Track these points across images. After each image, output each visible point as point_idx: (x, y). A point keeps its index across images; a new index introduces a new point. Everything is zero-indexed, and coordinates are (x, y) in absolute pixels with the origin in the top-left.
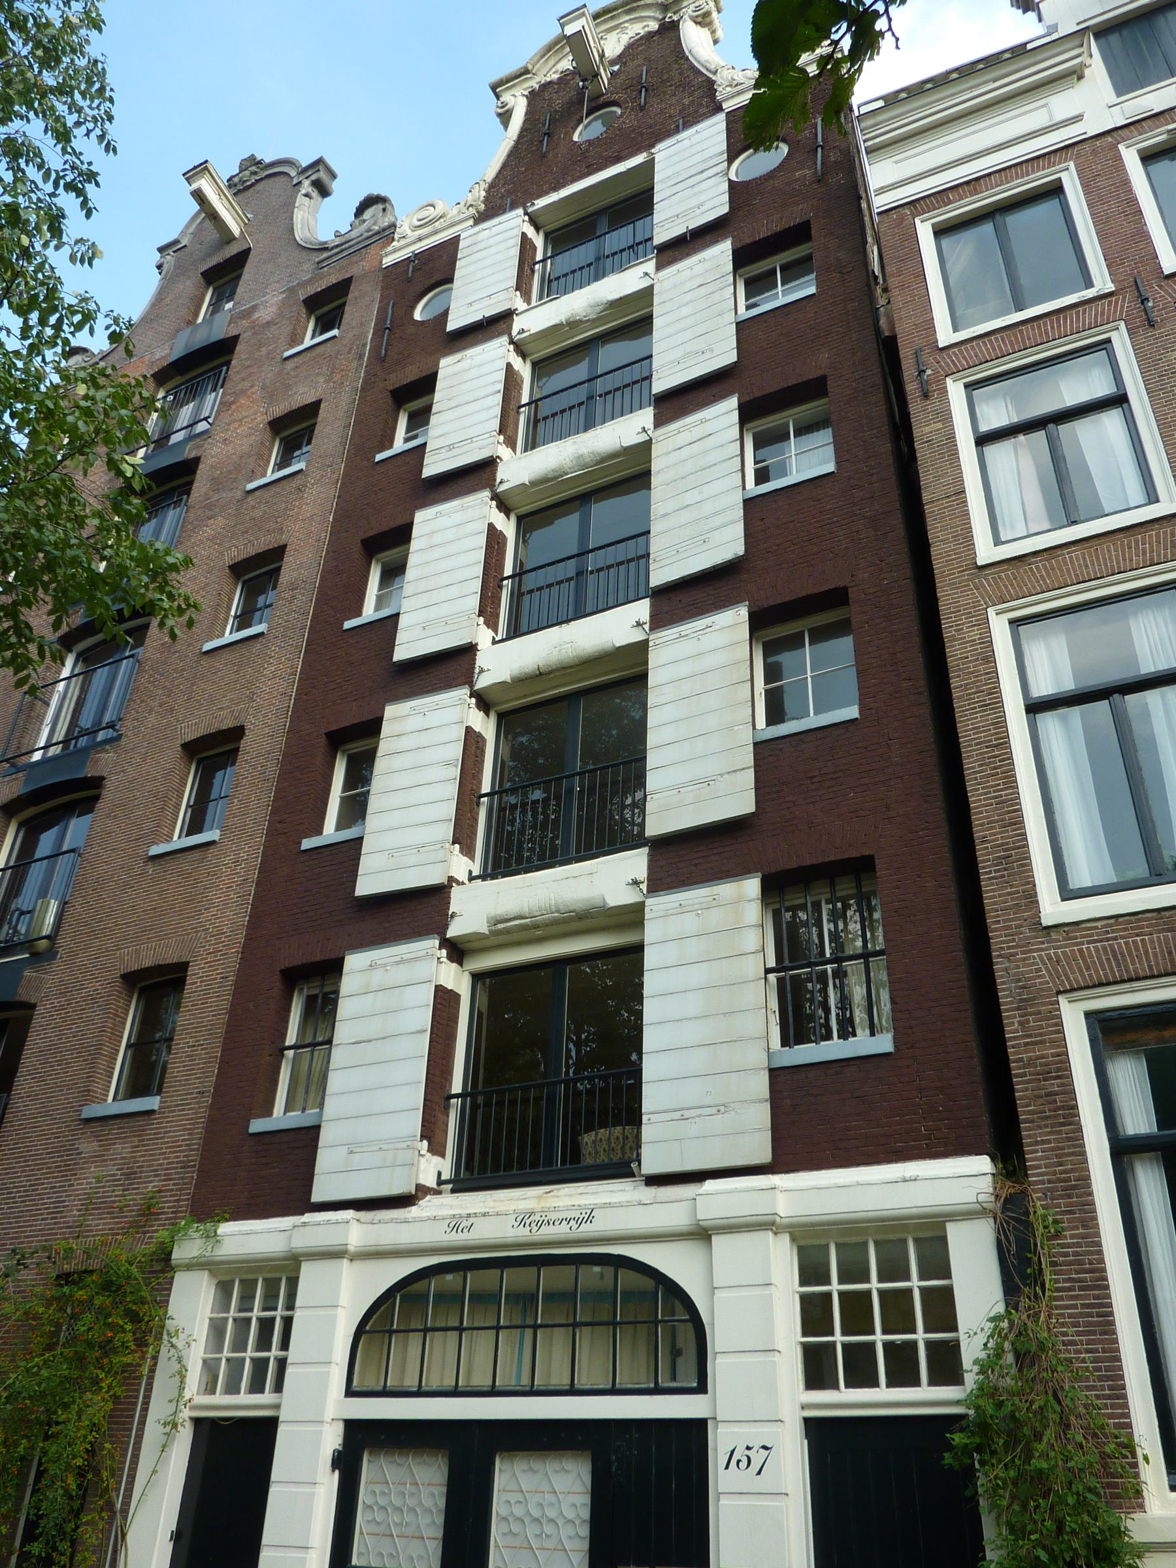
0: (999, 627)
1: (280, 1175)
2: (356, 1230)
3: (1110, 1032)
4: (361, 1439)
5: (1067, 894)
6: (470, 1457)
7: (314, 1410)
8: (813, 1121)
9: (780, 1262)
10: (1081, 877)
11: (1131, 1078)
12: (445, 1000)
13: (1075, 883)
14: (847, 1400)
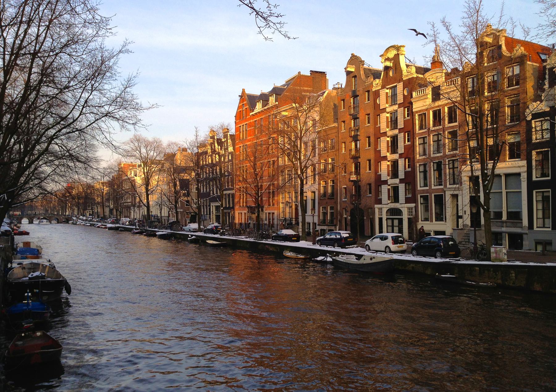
0: (417, 138)
1: (379, 202)
2: (385, 206)
3: (421, 197)
4: (387, 219)
5: (537, 227)
6: (393, 219)
7: (384, 217)
8: (408, 201)
9: (406, 209)
10: (422, 186)
11: (422, 199)
12: (389, 190)
13: (508, 194)
14: (409, 217)
